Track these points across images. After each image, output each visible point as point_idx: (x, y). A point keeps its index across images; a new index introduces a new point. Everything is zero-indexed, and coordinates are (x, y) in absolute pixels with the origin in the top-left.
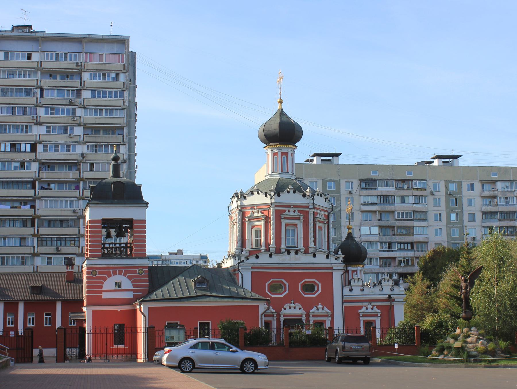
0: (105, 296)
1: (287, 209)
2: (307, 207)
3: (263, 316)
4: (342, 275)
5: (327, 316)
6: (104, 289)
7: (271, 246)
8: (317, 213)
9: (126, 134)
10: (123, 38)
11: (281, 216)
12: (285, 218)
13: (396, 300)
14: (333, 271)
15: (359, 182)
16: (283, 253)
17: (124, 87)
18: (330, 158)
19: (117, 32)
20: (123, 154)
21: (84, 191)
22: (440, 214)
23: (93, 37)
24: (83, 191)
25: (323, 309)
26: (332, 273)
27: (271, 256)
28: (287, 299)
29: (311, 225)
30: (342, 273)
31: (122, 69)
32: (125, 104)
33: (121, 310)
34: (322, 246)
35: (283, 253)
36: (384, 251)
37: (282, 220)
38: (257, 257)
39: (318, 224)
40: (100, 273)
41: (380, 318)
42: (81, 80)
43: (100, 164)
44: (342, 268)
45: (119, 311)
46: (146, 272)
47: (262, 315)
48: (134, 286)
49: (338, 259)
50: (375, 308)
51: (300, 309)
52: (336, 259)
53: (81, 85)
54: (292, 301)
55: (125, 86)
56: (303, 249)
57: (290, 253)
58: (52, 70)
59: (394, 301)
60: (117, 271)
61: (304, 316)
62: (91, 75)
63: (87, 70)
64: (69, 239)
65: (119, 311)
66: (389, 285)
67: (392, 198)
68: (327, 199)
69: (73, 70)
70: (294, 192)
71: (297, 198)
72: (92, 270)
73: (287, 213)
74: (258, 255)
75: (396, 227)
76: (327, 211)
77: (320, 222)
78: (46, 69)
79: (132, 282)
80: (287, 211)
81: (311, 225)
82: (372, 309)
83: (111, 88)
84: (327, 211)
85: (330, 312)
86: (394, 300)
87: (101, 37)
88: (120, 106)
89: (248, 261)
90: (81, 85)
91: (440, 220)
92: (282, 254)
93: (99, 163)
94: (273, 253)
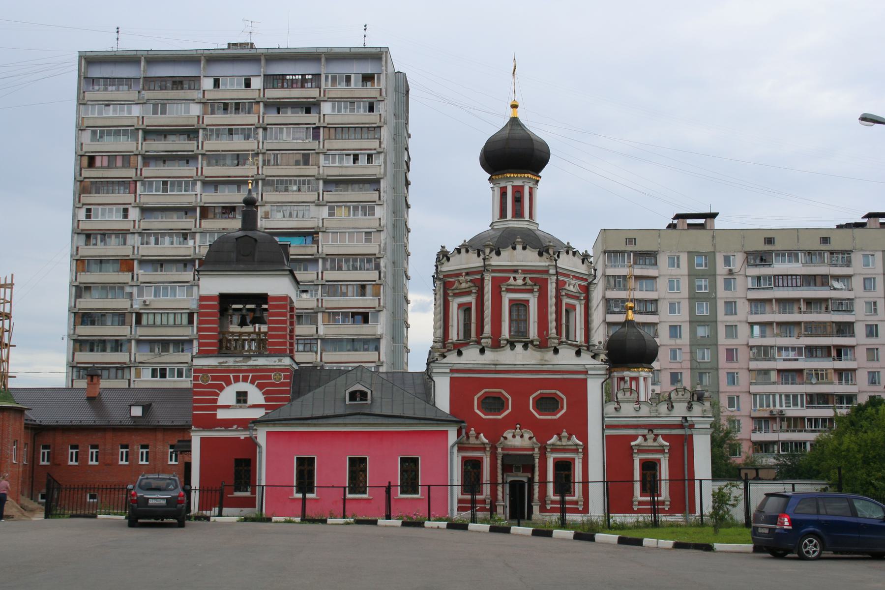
0: (221, 415)
1: (512, 275)
2: (546, 272)
3: (455, 449)
4: (603, 383)
5: (576, 451)
6: (219, 403)
7: (484, 335)
8: (565, 283)
9: (384, 188)
10: (378, 50)
11: (502, 286)
12: (508, 291)
13: (696, 426)
14: (588, 376)
15: (745, 255)
16: (503, 347)
17: (380, 121)
18: (702, 221)
19: (374, 42)
20: (380, 219)
21: (325, 272)
22: (875, 303)
23: (337, 50)
24: (322, 273)
25: (477, 437)
26: (586, 380)
27: (482, 351)
28: (510, 423)
29: (552, 301)
30: (603, 380)
31: (378, 95)
32: (383, 146)
33: (245, 438)
34: (575, 336)
35: (503, 347)
36: (790, 360)
37: (503, 293)
38: (460, 353)
39: (565, 300)
40: (214, 378)
41: (667, 455)
42: (320, 113)
43: (347, 233)
44: (603, 372)
45: (242, 437)
46: (286, 377)
47: (453, 446)
48: (266, 399)
49: (597, 357)
50: (660, 439)
51: (530, 438)
52: (594, 357)
53: (319, 121)
54: (518, 426)
55: (382, 120)
56: (537, 341)
57: (515, 346)
58: (278, 100)
59: (692, 426)
60: (240, 375)
61: (537, 450)
62: (333, 107)
63: (328, 98)
64: (302, 342)
65: (242, 437)
66: (684, 401)
67: (787, 279)
68: (586, 260)
69: (309, 100)
70: (524, 248)
71: (529, 258)
72: (201, 375)
73: (511, 281)
74: (461, 349)
75: (803, 324)
76: (586, 280)
77: (569, 296)
78: (271, 100)
79: (264, 394)
80: (512, 278)
81: (552, 301)
82: (655, 440)
83: (363, 124)
84: (586, 280)
85: (581, 443)
86: (693, 425)
87: (348, 50)
88: (375, 149)
89: (445, 360)
90: (319, 121)
91: (875, 310)
92: (502, 349)
93: (337, 232)
94: (487, 347)
